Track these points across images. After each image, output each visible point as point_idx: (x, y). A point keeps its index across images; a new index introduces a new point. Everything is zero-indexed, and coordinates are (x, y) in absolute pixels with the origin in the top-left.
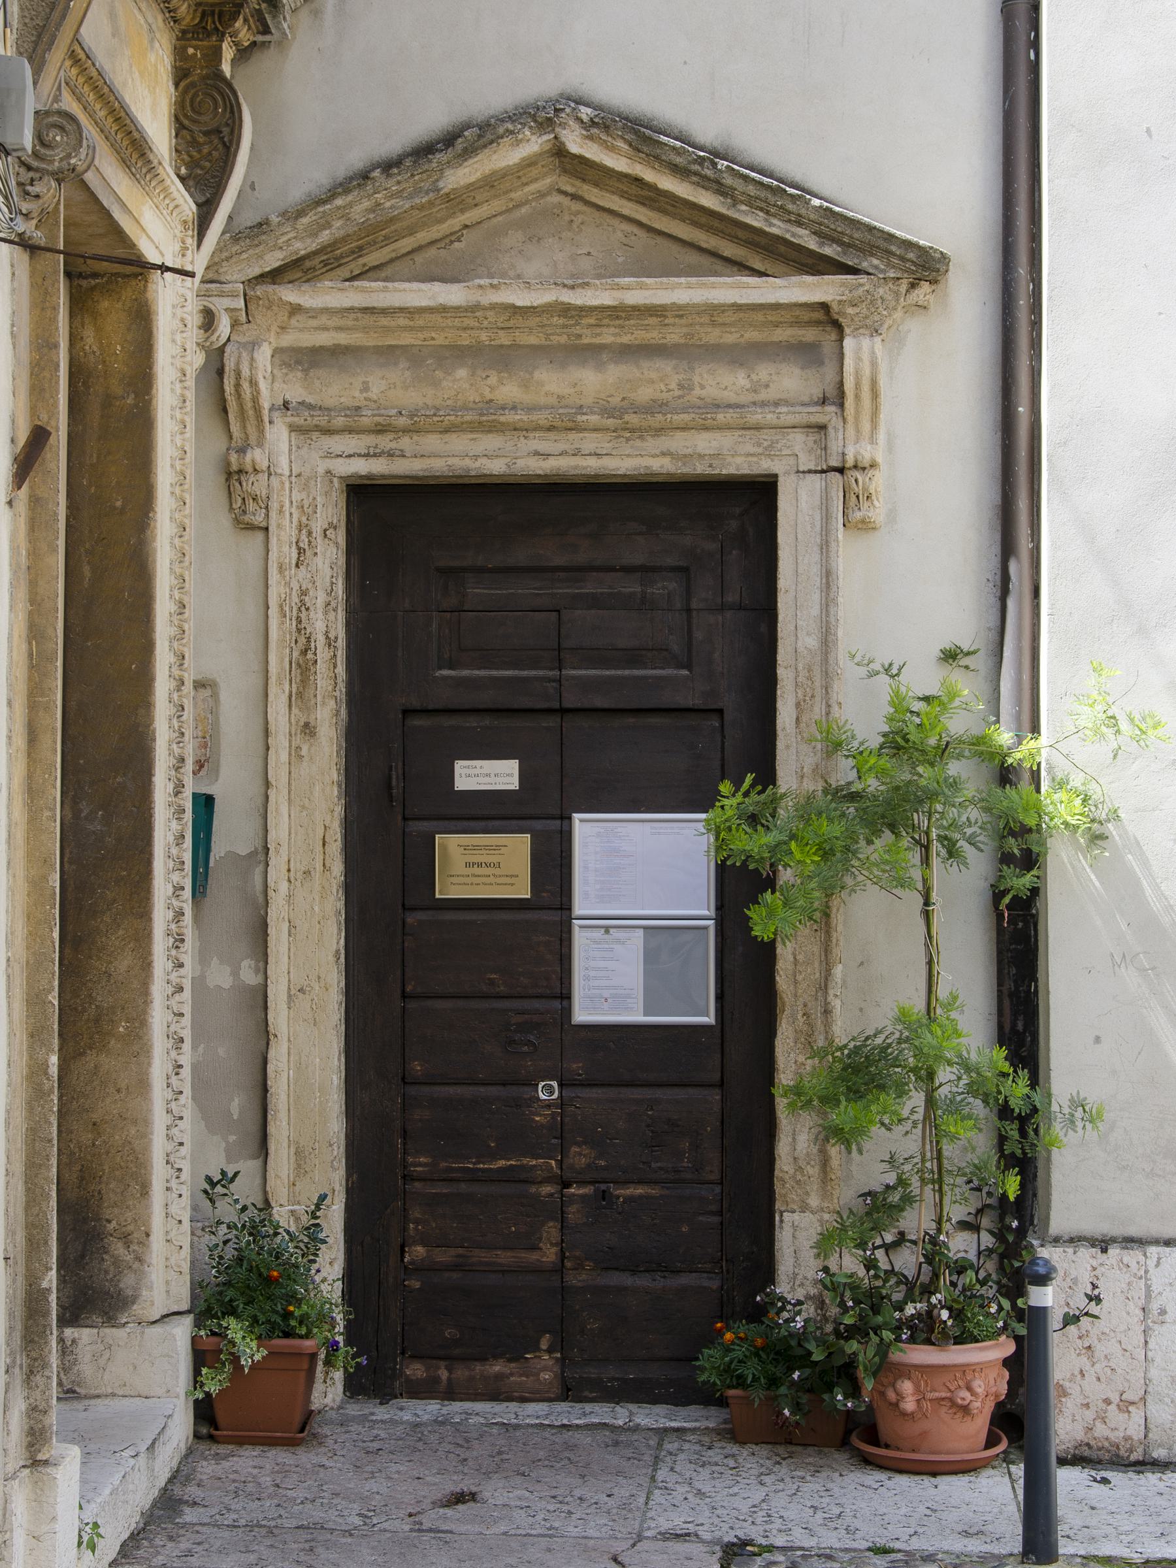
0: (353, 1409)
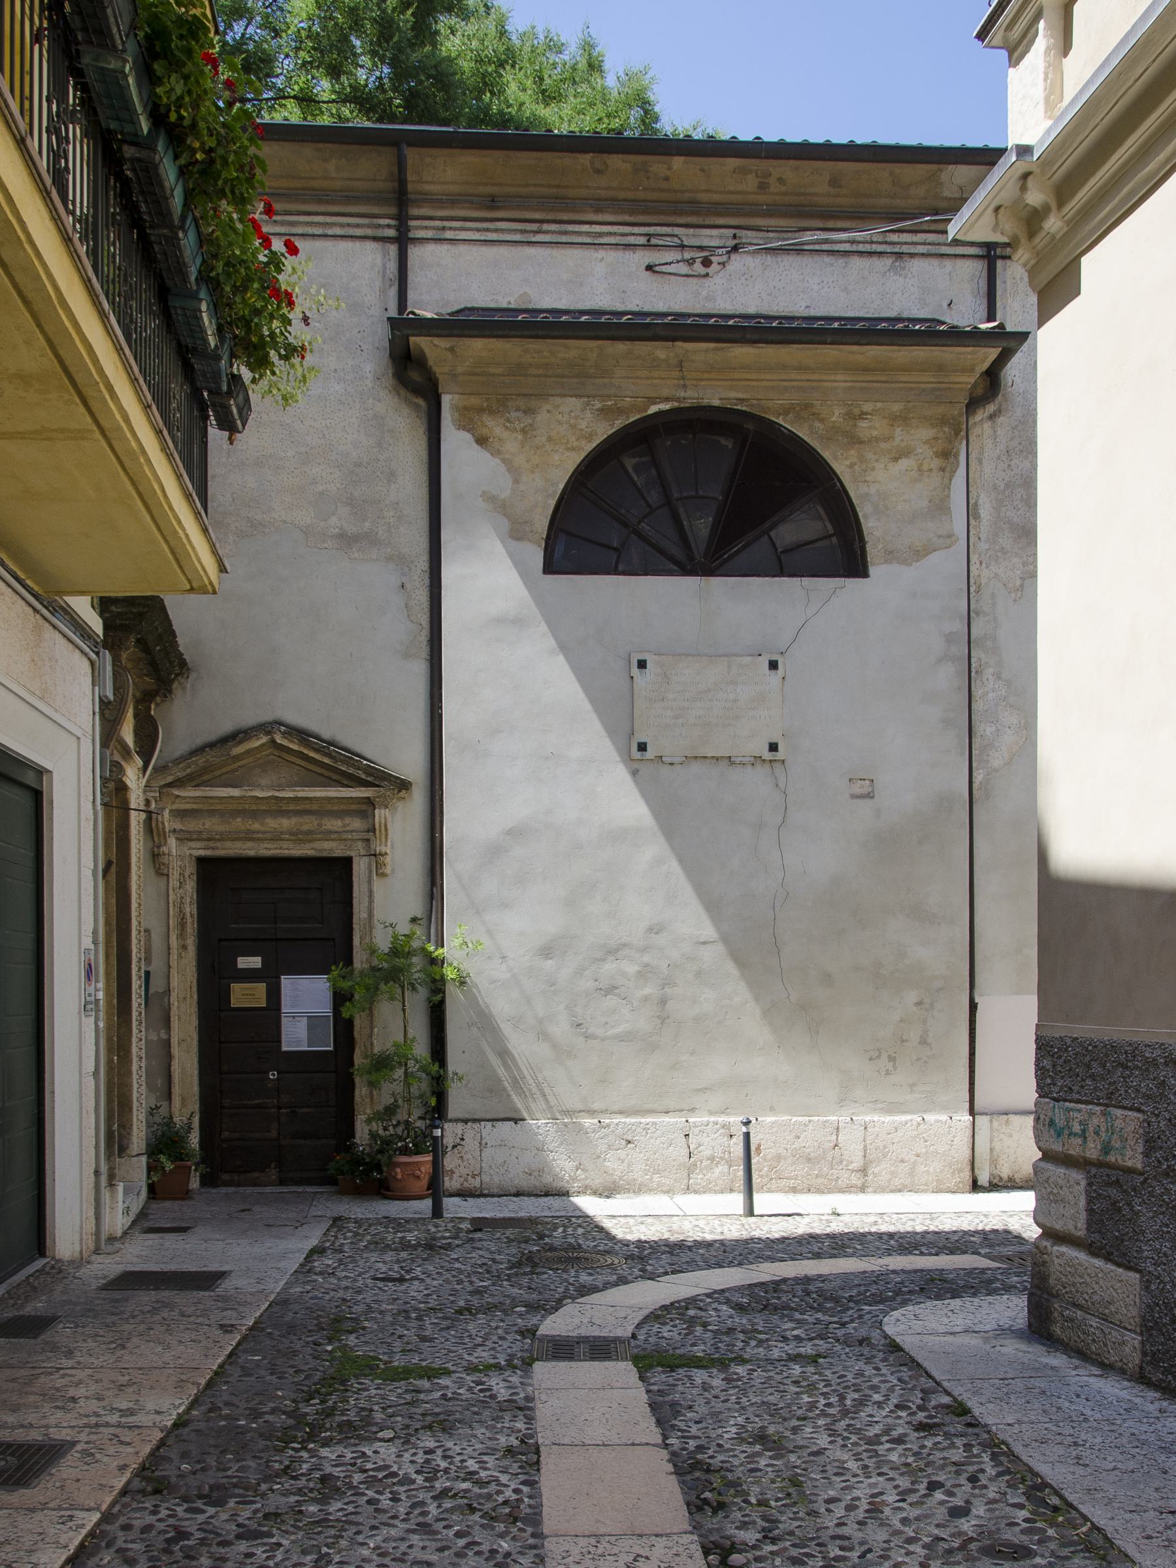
0: (203, 1190)
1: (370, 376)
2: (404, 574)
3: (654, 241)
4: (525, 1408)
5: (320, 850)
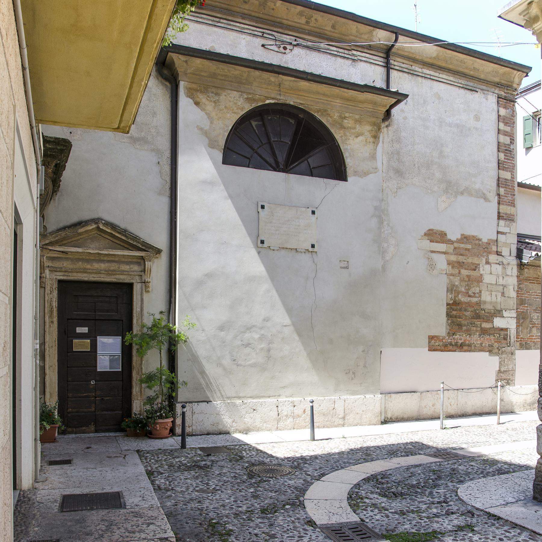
2: (159, 158)
3: (265, 35)
5: (119, 279)
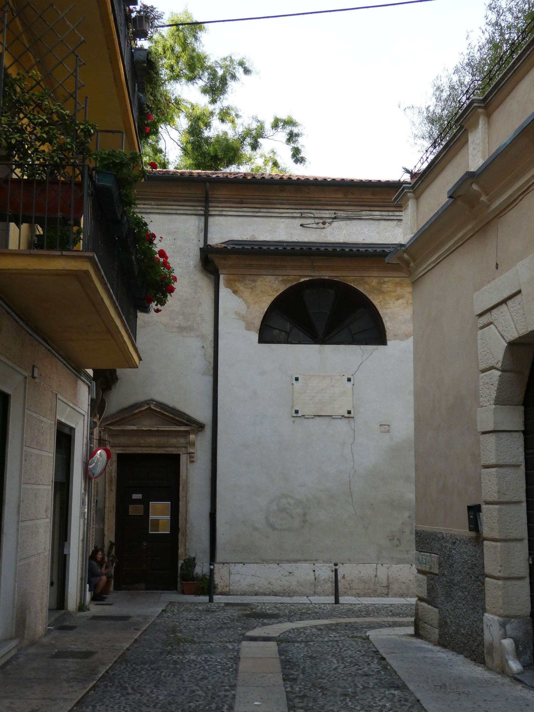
1: (192, 265)
3: (303, 215)
4: (238, 651)
